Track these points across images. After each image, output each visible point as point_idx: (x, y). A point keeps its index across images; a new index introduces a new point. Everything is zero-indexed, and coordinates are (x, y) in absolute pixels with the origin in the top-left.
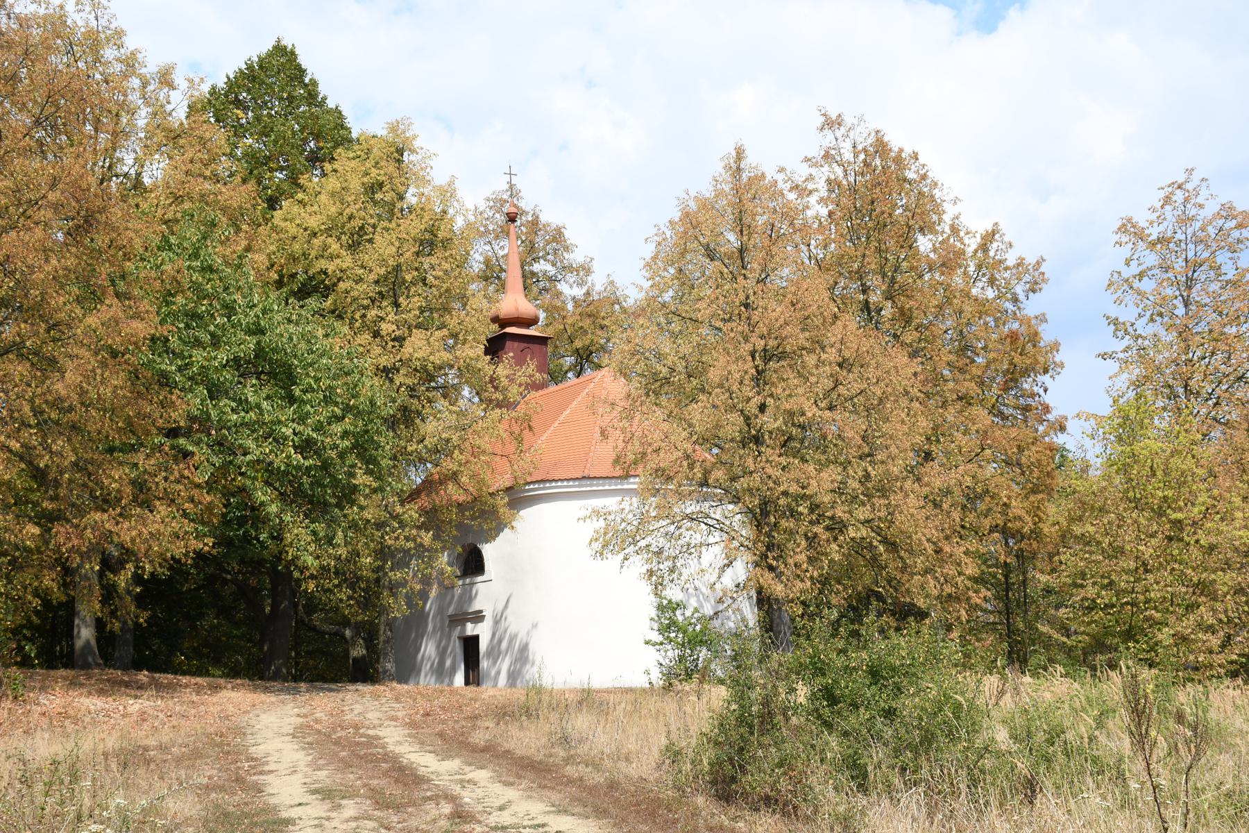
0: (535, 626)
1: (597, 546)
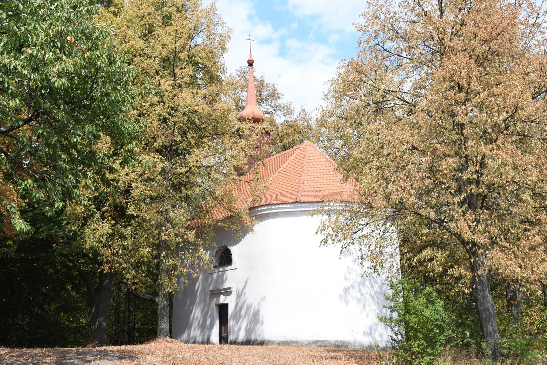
0: (264, 299)
1: (321, 237)
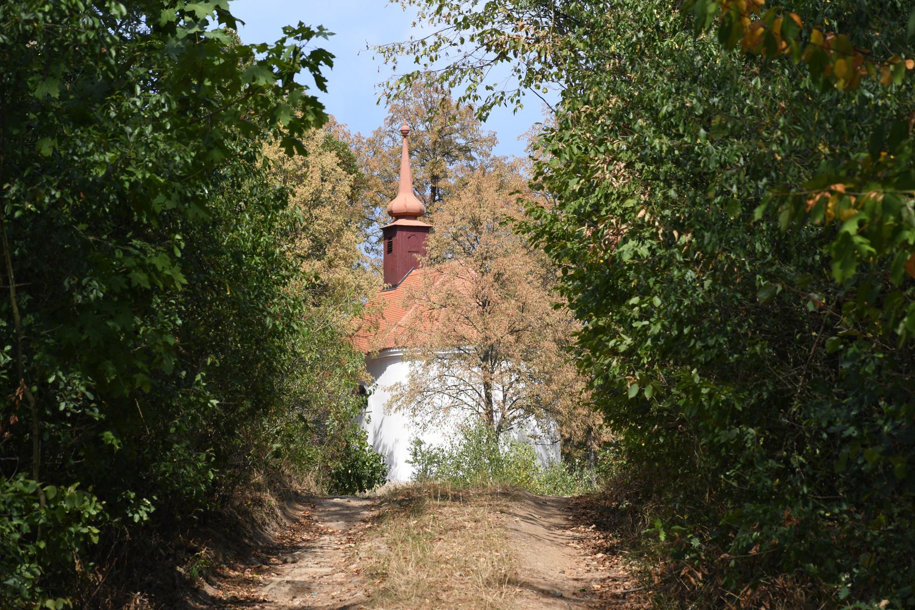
0: (397, 441)
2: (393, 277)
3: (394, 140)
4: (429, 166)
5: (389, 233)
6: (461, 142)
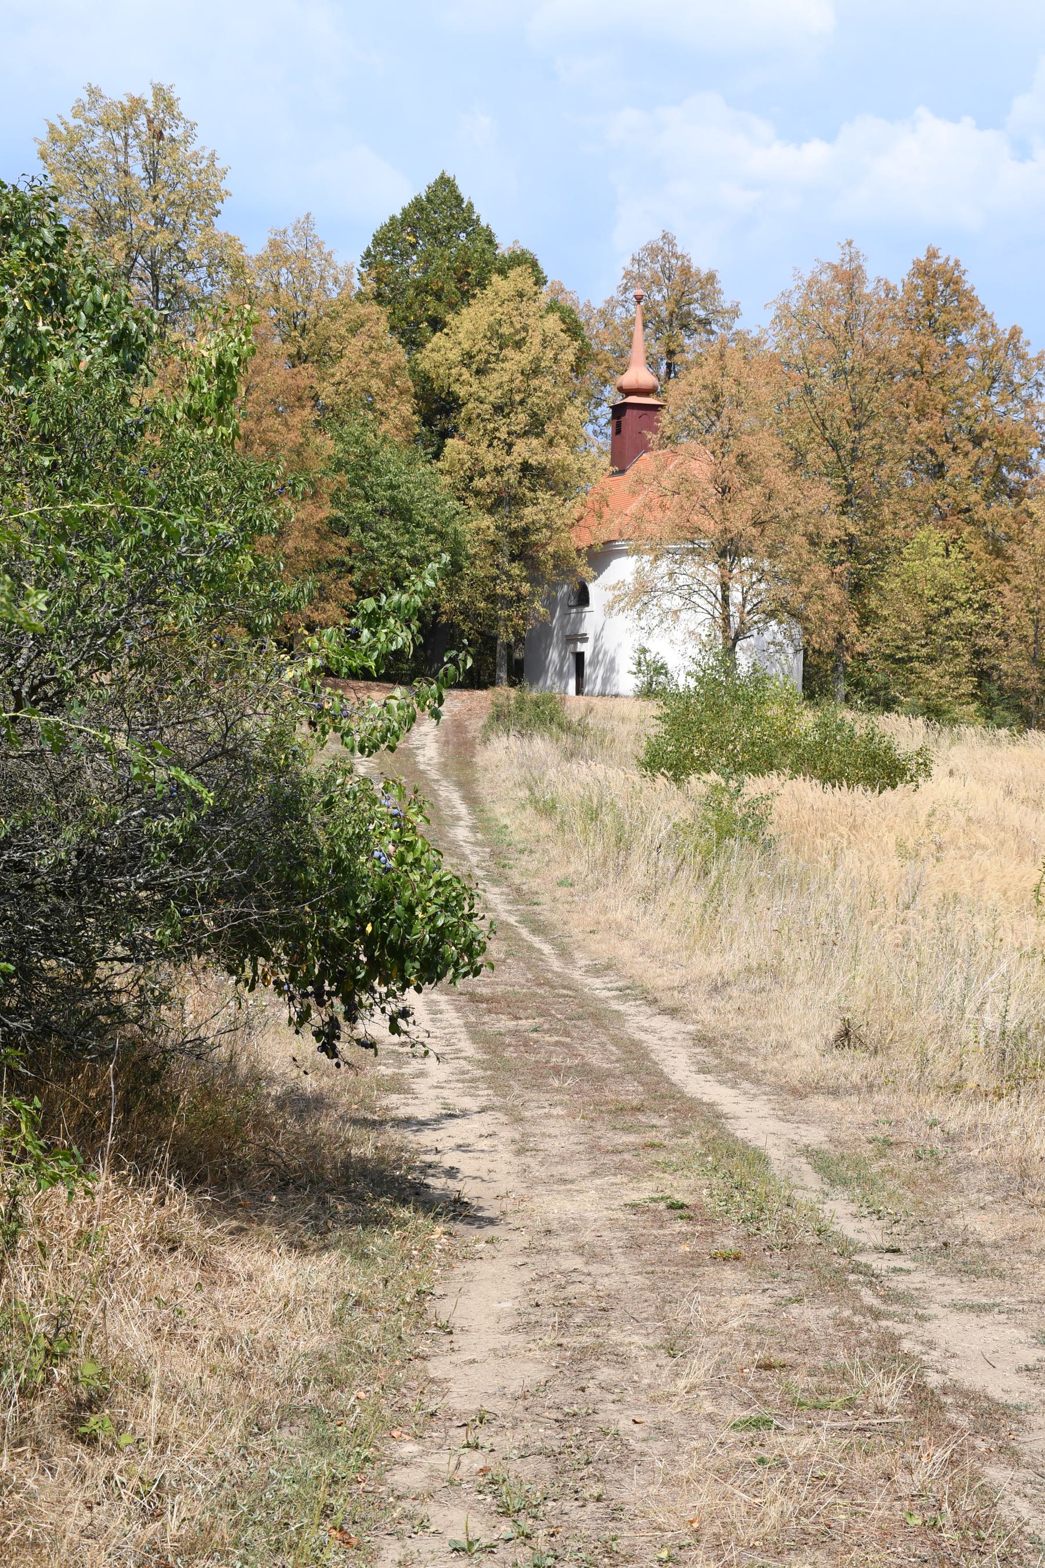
0: (619, 645)
2: (621, 462)
3: (628, 311)
4: (664, 340)
5: (618, 411)
6: (702, 313)
